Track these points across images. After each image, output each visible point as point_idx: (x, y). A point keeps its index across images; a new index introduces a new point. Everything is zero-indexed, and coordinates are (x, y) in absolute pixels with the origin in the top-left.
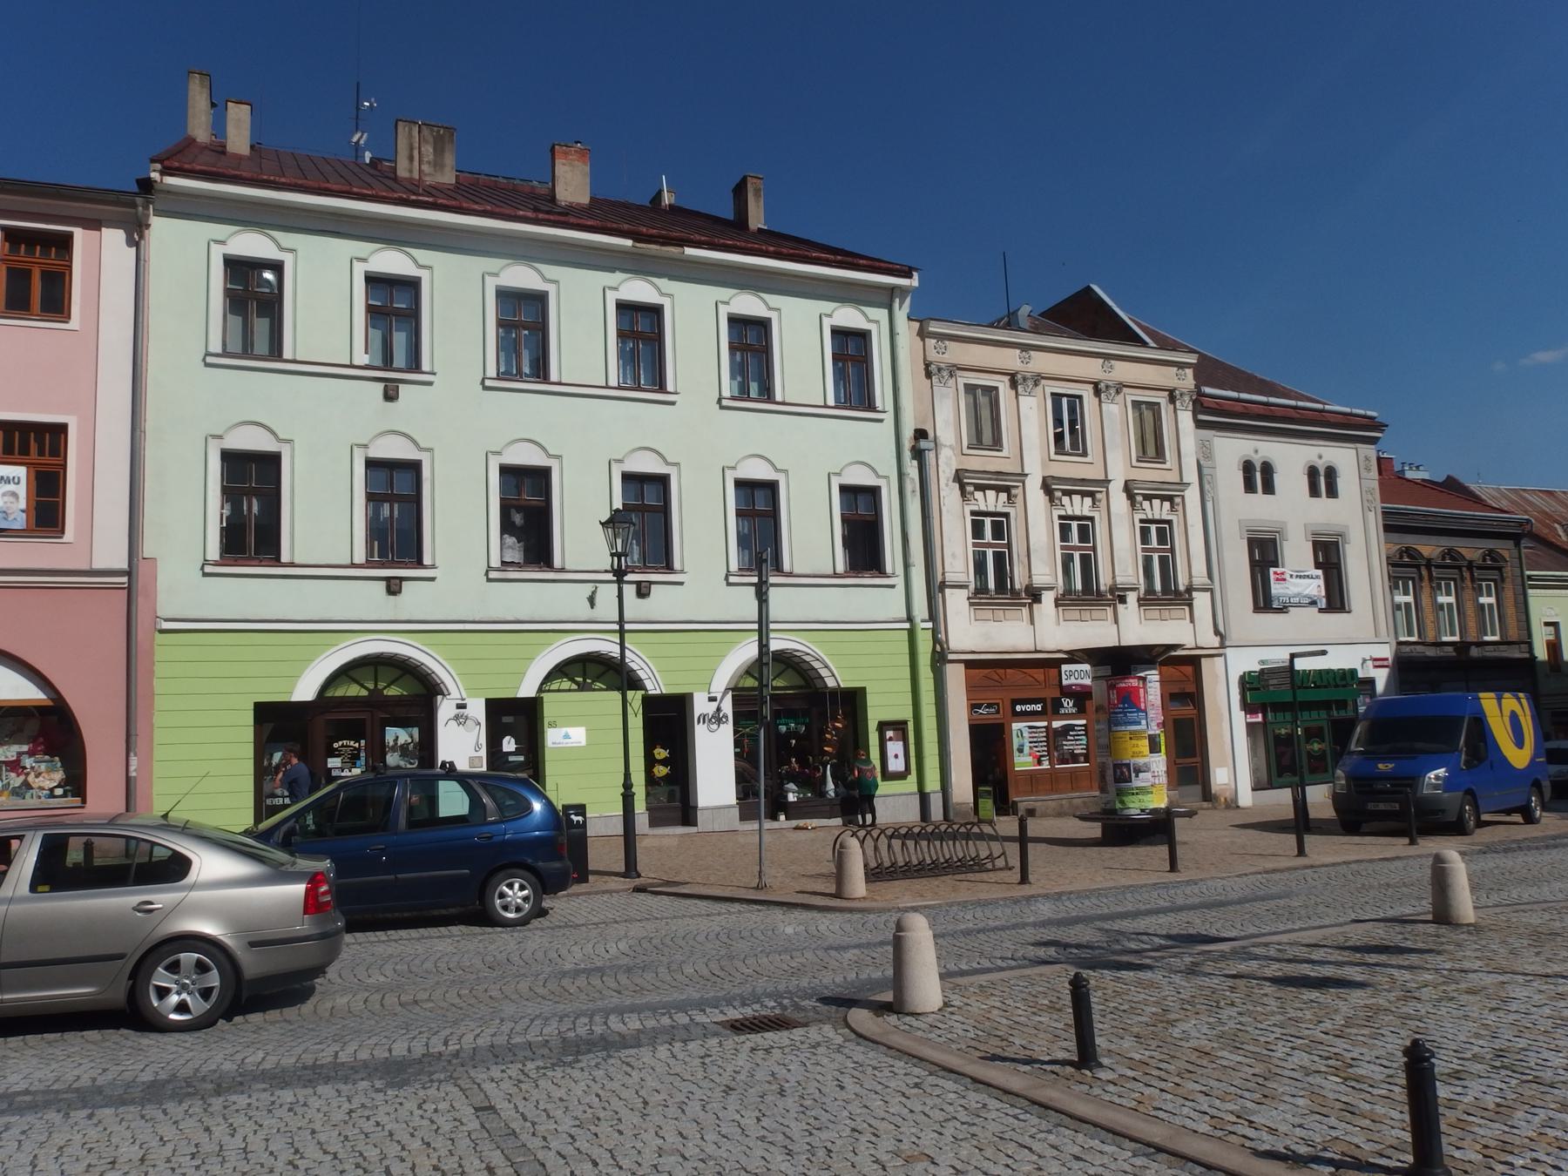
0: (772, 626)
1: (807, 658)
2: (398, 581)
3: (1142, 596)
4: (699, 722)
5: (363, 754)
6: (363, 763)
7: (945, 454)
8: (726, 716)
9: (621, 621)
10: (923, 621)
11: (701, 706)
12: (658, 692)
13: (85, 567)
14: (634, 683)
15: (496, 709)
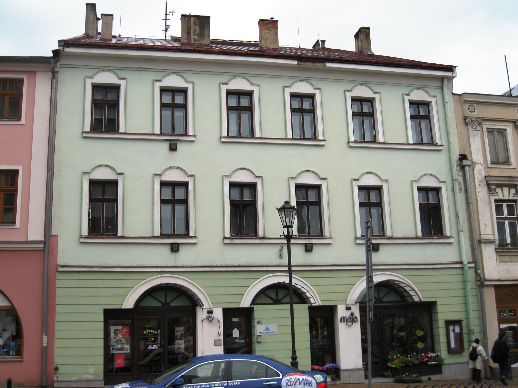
0: (365, 268)
1: (402, 285)
2: (177, 245)
3: (497, 247)
4: (341, 321)
5: (159, 337)
6: (159, 342)
7: (478, 168)
8: (356, 318)
9: (290, 266)
10: (469, 263)
11: (341, 312)
12: (317, 304)
13: (23, 240)
14: (302, 298)
15: (228, 313)
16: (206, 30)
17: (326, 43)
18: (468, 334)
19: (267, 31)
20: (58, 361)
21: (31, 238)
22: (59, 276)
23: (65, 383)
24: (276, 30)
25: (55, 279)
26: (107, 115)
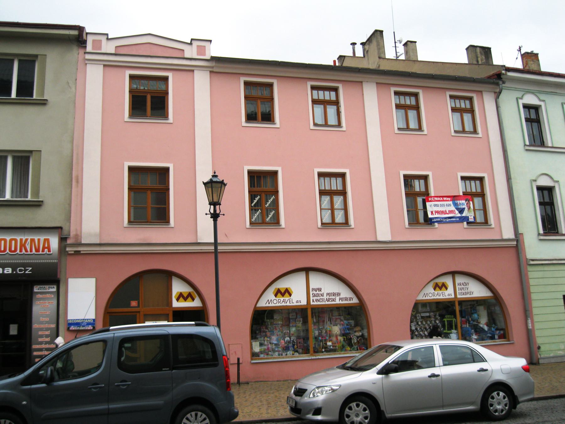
13: (499, 238)
16: (490, 59)
17: (419, 47)
18: (526, 311)
19: (532, 62)
20: (539, 341)
21: (505, 237)
22: (529, 268)
23: (546, 360)
24: (538, 62)
25: (527, 271)
26: (261, 108)
